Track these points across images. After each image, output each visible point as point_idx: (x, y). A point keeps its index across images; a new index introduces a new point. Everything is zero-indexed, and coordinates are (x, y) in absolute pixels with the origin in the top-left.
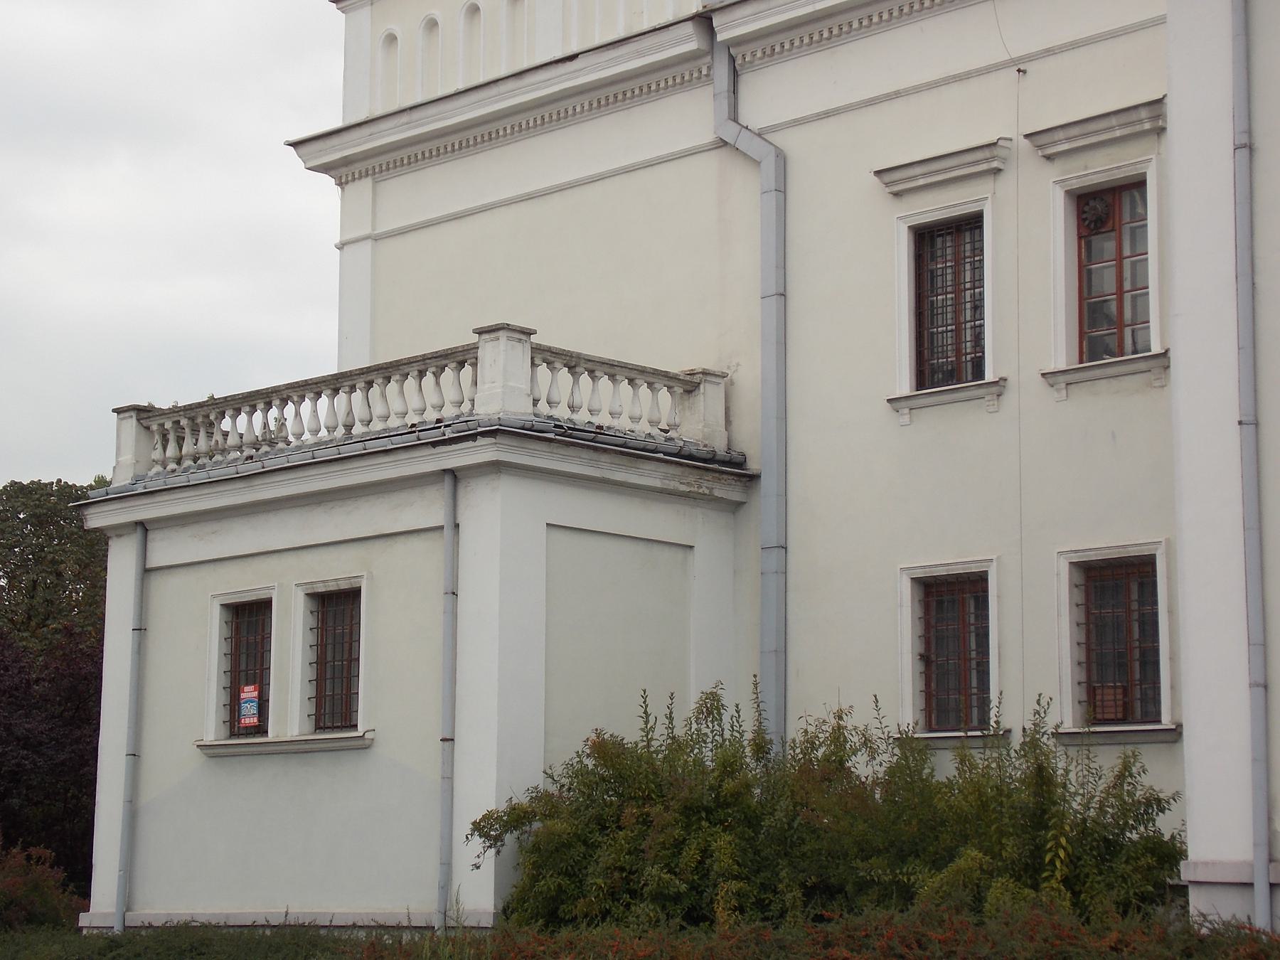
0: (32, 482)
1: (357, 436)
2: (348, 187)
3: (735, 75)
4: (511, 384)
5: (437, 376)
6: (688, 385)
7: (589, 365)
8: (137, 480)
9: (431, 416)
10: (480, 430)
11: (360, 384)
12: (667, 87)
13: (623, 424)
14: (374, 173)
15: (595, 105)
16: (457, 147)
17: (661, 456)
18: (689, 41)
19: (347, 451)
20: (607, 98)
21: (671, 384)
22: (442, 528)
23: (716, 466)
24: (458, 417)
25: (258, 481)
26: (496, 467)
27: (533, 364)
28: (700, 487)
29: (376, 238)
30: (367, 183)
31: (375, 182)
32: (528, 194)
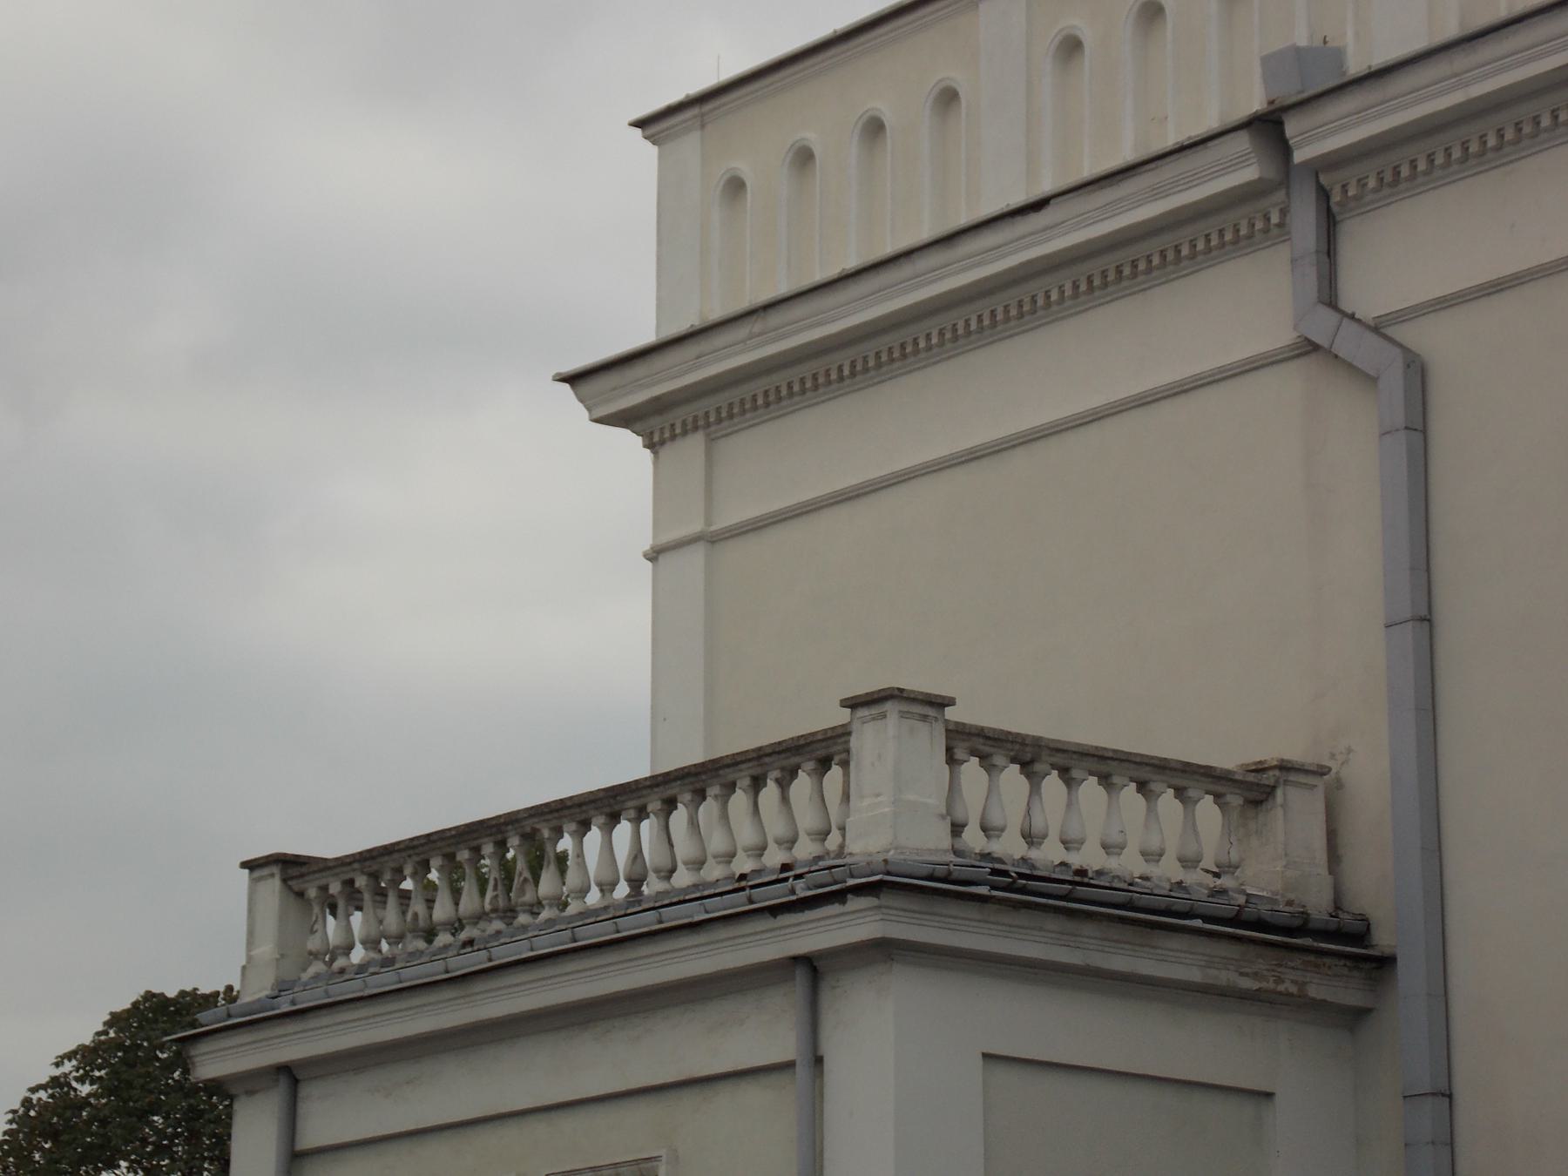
0: (183, 994)
1: (649, 898)
2: (665, 452)
3: (1330, 224)
4: (911, 797)
5: (784, 785)
6: (1253, 790)
7: (1059, 759)
8: (282, 988)
9: (775, 858)
10: (851, 882)
11: (654, 805)
12: (1208, 250)
13: (1129, 864)
14: (708, 425)
15: (1083, 287)
16: (846, 372)
17: (1198, 923)
18: (1241, 167)
19: (630, 926)
20: (1104, 274)
21: (1220, 789)
22: (789, 1066)
23: (1307, 941)
24: (819, 858)
25: (479, 986)
26: (882, 951)
27: (952, 760)
28: (1279, 981)
29: (713, 539)
30: (696, 442)
31: (711, 440)
32: (971, 451)
